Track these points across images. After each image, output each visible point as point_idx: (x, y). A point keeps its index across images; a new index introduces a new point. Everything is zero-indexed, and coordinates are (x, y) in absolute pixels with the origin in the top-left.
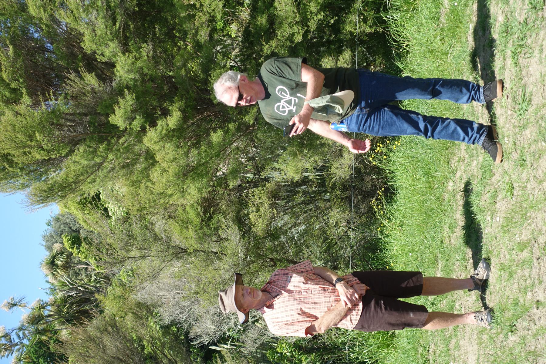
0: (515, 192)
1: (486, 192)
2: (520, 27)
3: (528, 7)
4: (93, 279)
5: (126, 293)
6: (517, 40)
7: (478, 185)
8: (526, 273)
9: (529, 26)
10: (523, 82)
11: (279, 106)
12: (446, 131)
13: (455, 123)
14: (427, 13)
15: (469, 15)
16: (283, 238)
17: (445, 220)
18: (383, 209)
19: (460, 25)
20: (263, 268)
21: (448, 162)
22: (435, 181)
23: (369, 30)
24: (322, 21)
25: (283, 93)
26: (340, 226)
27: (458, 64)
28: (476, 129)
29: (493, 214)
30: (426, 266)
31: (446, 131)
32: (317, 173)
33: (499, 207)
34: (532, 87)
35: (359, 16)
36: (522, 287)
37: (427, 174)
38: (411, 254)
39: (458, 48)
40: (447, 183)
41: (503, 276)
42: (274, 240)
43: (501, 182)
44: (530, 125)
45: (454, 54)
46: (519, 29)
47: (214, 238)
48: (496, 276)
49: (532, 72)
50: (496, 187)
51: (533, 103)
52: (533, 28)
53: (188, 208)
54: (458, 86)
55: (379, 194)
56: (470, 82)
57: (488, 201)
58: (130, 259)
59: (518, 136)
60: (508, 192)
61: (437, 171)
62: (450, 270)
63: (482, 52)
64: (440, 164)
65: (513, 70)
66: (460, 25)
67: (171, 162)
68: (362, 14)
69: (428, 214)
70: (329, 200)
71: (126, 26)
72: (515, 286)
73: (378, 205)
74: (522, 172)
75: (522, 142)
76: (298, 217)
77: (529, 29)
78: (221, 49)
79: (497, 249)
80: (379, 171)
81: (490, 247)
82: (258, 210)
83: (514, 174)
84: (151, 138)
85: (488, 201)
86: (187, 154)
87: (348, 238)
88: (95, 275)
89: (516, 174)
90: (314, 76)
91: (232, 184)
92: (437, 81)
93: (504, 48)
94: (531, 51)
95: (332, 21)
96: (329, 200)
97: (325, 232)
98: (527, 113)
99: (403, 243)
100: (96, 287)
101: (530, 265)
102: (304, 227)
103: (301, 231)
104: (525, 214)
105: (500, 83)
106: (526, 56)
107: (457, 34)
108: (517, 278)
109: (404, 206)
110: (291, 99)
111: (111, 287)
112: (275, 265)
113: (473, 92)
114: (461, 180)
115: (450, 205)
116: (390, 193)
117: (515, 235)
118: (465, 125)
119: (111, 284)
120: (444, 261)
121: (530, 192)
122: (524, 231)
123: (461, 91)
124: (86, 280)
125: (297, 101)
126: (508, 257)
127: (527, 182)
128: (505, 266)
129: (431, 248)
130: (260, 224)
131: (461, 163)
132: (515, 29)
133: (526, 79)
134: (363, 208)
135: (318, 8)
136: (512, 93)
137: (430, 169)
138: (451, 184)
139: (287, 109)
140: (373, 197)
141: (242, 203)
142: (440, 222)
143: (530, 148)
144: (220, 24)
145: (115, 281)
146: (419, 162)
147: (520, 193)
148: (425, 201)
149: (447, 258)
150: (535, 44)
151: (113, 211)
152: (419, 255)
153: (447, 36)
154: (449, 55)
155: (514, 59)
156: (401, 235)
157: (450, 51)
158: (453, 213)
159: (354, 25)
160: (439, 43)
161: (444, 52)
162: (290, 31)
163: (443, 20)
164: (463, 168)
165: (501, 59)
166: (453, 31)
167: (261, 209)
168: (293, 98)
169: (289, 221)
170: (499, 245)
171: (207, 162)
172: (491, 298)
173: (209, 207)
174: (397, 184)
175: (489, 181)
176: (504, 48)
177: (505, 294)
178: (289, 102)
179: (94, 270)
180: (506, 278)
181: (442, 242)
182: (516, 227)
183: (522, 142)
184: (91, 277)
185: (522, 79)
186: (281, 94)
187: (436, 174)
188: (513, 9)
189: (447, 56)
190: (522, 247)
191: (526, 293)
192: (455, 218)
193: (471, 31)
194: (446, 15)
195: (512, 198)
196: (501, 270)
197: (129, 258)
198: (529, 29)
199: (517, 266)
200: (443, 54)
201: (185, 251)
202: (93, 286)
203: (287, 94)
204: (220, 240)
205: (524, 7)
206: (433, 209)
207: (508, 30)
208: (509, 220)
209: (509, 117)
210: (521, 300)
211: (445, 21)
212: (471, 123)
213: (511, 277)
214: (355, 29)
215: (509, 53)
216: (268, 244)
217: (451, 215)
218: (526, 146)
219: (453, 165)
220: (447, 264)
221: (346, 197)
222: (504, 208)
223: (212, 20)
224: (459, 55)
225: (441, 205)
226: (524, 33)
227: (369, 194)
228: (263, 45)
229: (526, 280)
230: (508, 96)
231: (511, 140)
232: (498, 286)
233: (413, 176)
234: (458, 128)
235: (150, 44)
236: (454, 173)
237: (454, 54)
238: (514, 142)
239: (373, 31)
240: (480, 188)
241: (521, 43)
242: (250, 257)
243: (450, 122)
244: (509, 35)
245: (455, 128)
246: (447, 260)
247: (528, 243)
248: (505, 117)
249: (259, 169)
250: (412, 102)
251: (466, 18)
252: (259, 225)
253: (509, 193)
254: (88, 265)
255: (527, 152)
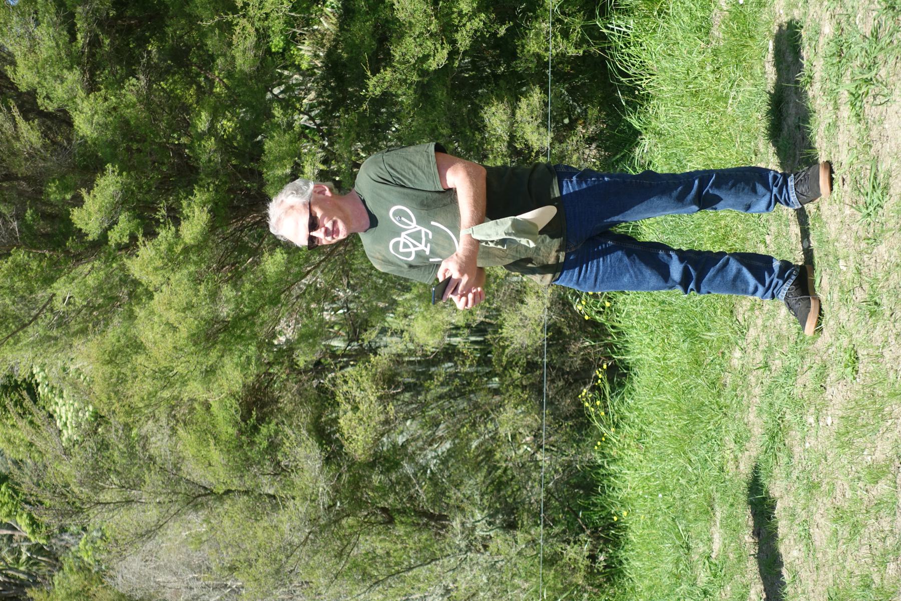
0: (861, 366)
1: (806, 367)
2: (866, 45)
3: (879, 7)
4: (24, 557)
5: (92, 585)
6: (860, 70)
7: (789, 356)
8: (884, 524)
9: (883, 43)
10: (872, 152)
11: (398, 243)
12: (723, 277)
13: (738, 260)
14: (686, 18)
15: (768, 23)
16: (408, 469)
17: (727, 427)
18: (606, 407)
19: (751, 43)
20: (366, 526)
21: (732, 312)
22: (707, 348)
23: (572, 51)
24: (482, 33)
25: (403, 219)
26: (520, 445)
27: (747, 119)
28: (776, 270)
29: (819, 411)
30: (691, 517)
31: (723, 277)
32: (473, 339)
33: (830, 397)
34: (889, 160)
35: (553, 24)
36: (878, 553)
37: (691, 335)
38: (660, 495)
39: (747, 86)
40: (730, 352)
41: (840, 533)
42: (388, 470)
43: (834, 349)
44: (888, 235)
45: (740, 98)
46: (862, 48)
47: (268, 467)
48: (828, 533)
49: (889, 133)
50: (824, 358)
51: (892, 191)
52: (890, 47)
53: (215, 409)
54: (745, 182)
55: (597, 378)
56: (767, 171)
57: (810, 386)
58: (99, 507)
59: (865, 257)
60: (847, 366)
61: (709, 330)
62: (738, 524)
63: (793, 94)
64: (716, 316)
65: (854, 129)
66: (751, 43)
67: (184, 310)
68: (560, 21)
69: (694, 414)
70: (496, 392)
71: (94, 43)
72: (864, 550)
73: (593, 400)
74: (874, 328)
75: (873, 268)
76: (435, 423)
77: (882, 49)
78: (282, 92)
79: (828, 480)
80: (595, 329)
81: (814, 476)
82: (356, 409)
83: (858, 332)
84: (143, 264)
85: (810, 386)
86: (214, 296)
87: (538, 467)
88: (28, 550)
89: (863, 332)
90: (469, 174)
91: (303, 359)
92: (704, 176)
93: (835, 87)
94: (886, 91)
95: (502, 31)
96: (496, 392)
97: (490, 453)
98: (880, 211)
99: (645, 474)
100: (29, 574)
101: (892, 509)
102: (448, 445)
103: (443, 453)
104: (881, 410)
105: (825, 168)
106: (878, 102)
107: (745, 60)
108: (867, 535)
109: (646, 401)
110: (420, 231)
111: (61, 574)
112: (391, 521)
113: (775, 190)
114: (757, 345)
115: (736, 396)
116: (619, 374)
117: (863, 451)
118: (759, 265)
119: (61, 568)
120: (727, 507)
121: (889, 365)
122: (879, 443)
123: (754, 191)
124: (9, 560)
125: (430, 237)
126: (849, 494)
127: (884, 346)
128: (844, 512)
129: (700, 481)
130: (360, 437)
131: (757, 312)
132: (856, 49)
133: (879, 145)
134: (566, 403)
135: (475, 5)
136: (851, 173)
137: (695, 326)
138: (738, 354)
139: (413, 250)
140: (585, 384)
141: (326, 398)
142: (718, 429)
143: (887, 280)
144: (277, 43)
145: (68, 561)
146: (676, 311)
147: (871, 368)
148: (687, 390)
149: (731, 500)
150: (895, 78)
151: (64, 419)
152: (678, 496)
153: (726, 63)
154: (730, 101)
155: (853, 105)
156: (641, 457)
157: (732, 94)
158: (742, 411)
159: (543, 41)
160: (711, 77)
161: (719, 94)
162: (419, 48)
163: (716, 34)
164: (760, 322)
165: (831, 108)
166: (737, 53)
167: (361, 407)
168: (424, 230)
169: (420, 432)
170: (833, 473)
171: (254, 314)
172: (818, 575)
173: (257, 404)
174: (629, 358)
175: (810, 347)
176: (835, 87)
177: (844, 567)
178: (416, 236)
179: (27, 539)
180: (847, 535)
181: (722, 469)
182: (865, 435)
183: (873, 268)
184: (20, 553)
185: (871, 146)
186: (400, 221)
187: (708, 335)
188: (850, 10)
189: (727, 103)
190: (876, 474)
191: (884, 564)
192: (746, 420)
193: (770, 56)
194: (724, 22)
195: (855, 378)
196: (835, 521)
197: (99, 503)
198: (882, 49)
199: (868, 512)
200: (718, 99)
201: (208, 492)
202: (23, 573)
203: (412, 221)
204: (280, 471)
205: (872, 7)
206: (702, 404)
207: (842, 50)
208: (850, 422)
209: (847, 221)
210: (877, 579)
211: (721, 35)
212: (769, 260)
213: (855, 534)
214: (547, 50)
215: (845, 96)
216: (377, 479)
217: (738, 415)
218: (880, 276)
219: (740, 318)
220: (731, 513)
221: (532, 385)
222: (840, 398)
223: (263, 36)
224: (750, 100)
225: (719, 396)
226: (873, 56)
227: (577, 377)
228: (369, 79)
229: (885, 538)
230: (844, 180)
231: (852, 265)
232: (831, 553)
233: (663, 339)
234: (745, 271)
235: (142, 77)
236: (742, 332)
237: (740, 98)
238: (857, 269)
239: (581, 52)
240: (793, 360)
241: (868, 76)
242: (342, 503)
243: (728, 260)
244: (844, 60)
245: (739, 272)
246: (732, 505)
247: (888, 467)
248: (838, 220)
249: (356, 326)
250: (653, 226)
251: (761, 29)
252: (357, 434)
253: (850, 369)
254: (14, 529)
255: (883, 287)
